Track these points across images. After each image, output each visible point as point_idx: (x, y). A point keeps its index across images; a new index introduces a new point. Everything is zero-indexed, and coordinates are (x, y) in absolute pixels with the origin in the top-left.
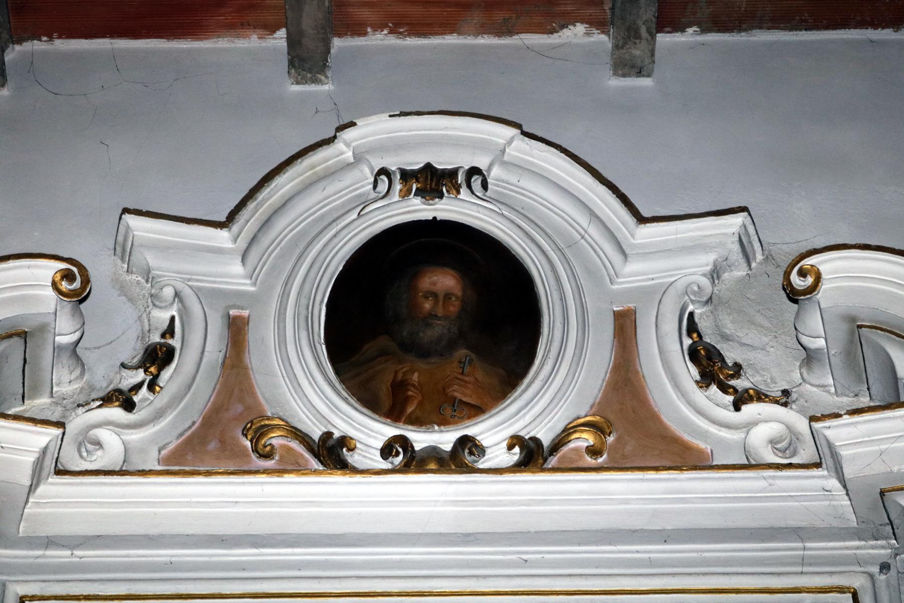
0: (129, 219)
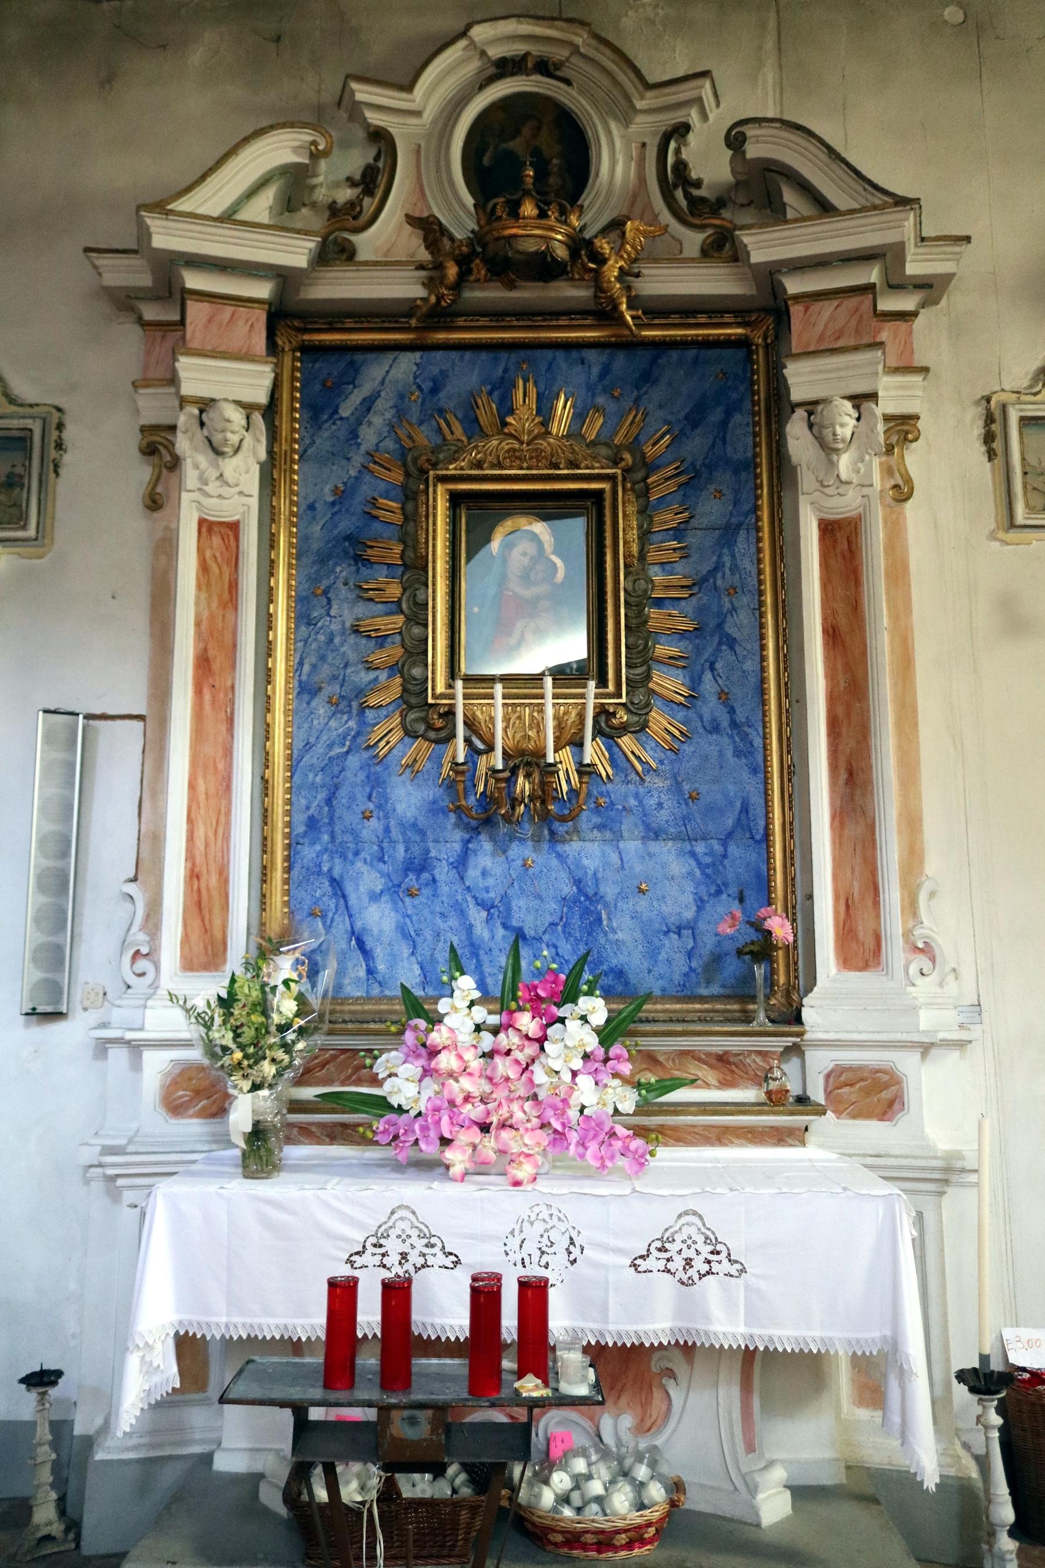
0: (354, 85)
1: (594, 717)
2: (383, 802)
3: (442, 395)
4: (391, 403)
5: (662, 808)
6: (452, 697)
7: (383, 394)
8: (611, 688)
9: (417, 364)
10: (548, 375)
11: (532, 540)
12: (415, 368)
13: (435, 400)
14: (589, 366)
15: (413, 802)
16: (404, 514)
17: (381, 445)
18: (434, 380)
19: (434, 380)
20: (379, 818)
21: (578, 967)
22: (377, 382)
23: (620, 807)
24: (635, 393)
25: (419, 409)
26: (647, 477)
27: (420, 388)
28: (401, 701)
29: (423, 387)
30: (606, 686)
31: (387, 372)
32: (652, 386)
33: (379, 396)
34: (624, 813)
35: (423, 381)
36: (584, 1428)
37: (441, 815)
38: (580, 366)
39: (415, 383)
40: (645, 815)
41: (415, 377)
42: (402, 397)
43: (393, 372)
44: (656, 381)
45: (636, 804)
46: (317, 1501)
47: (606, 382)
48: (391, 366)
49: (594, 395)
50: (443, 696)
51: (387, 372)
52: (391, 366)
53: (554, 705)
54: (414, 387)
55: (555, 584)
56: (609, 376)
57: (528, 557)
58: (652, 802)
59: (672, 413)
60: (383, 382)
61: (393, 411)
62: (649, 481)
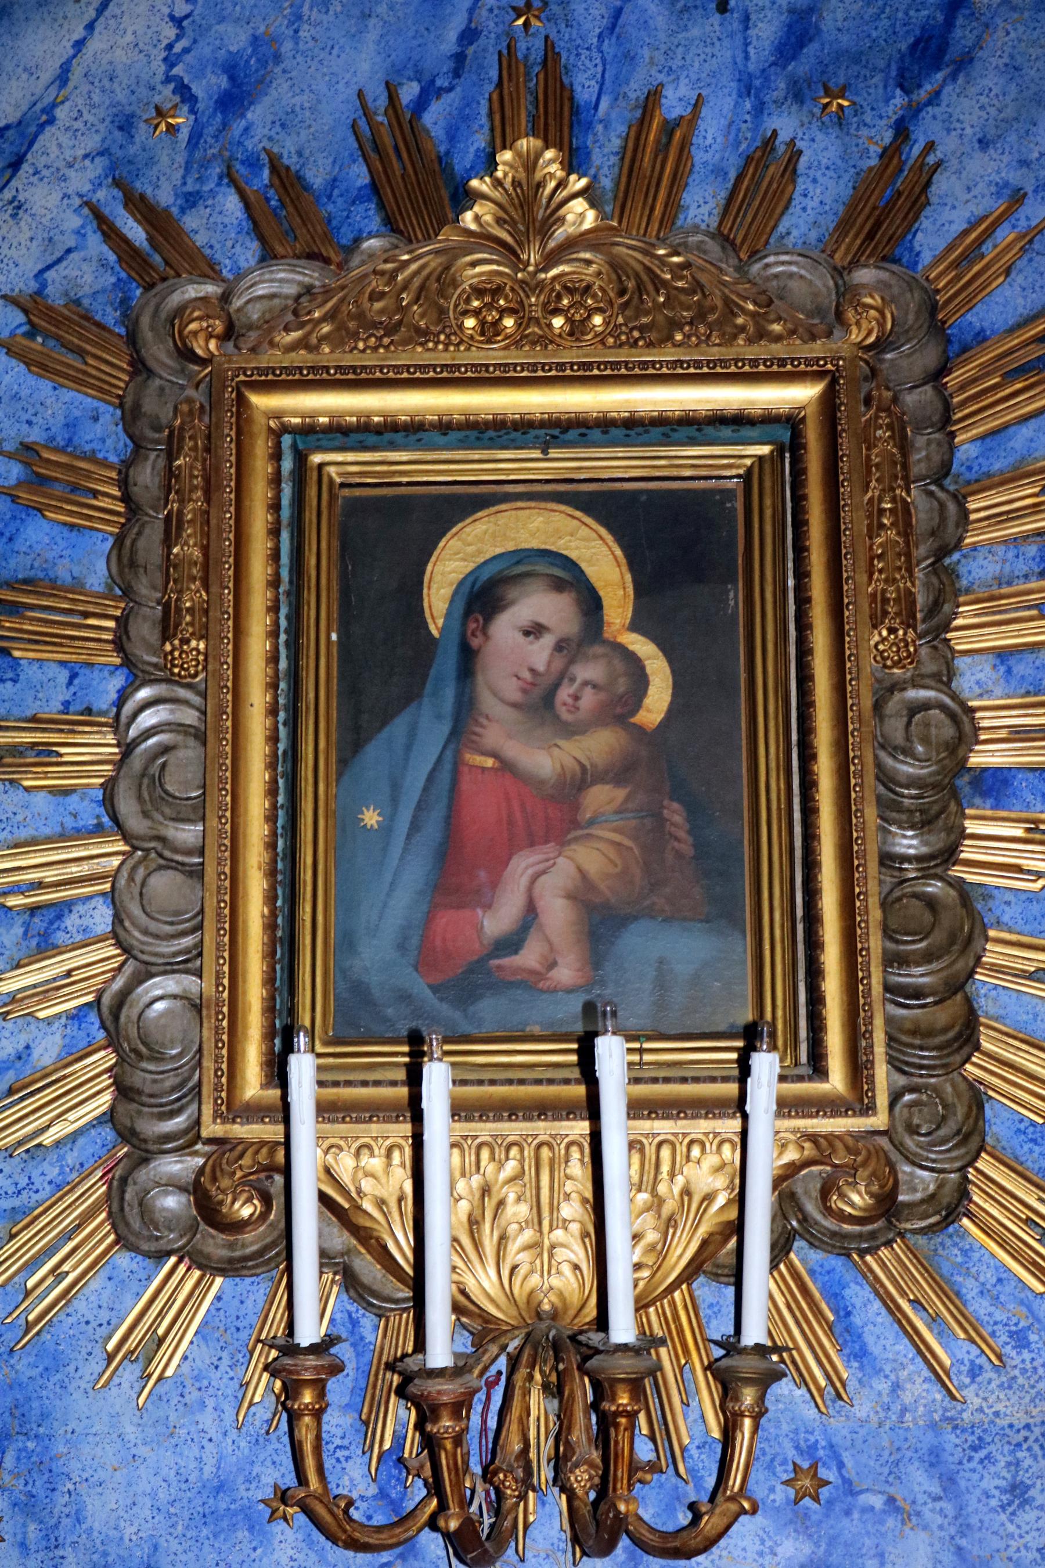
1: (777, 1182)
2: (39, 1488)
3: (257, 114)
4: (92, 142)
5: (1026, 1502)
6: (284, 1112)
7: (61, 113)
8: (837, 1081)
9: (178, 22)
10: (609, 47)
11: (558, 585)
12: (170, 32)
13: (237, 127)
14: (747, 18)
15: (144, 1486)
16: (126, 498)
17: (50, 275)
18: (231, 68)
19: (231, 68)
20: (23, 1545)
21: (447, 766)
22: (47, 74)
23: (877, 1502)
24: (899, 99)
25: (180, 159)
26: (943, 370)
27: (184, 92)
28: (108, 1133)
29: (197, 89)
30: (818, 1068)
31: (79, 45)
32: (953, 77)
33: (51, 121)
34: (891, 1522)
35: (200, 74)
36: (495, 694)
37: (242, 1534)
38: (716, 19)
39: (168, 79)
40: (965, 1530)
41: (170, 62)
42: (125, 124)
43: (96, 44)
44: (964, 63)
45: (936, 1489)
46: (652, 727)
47: (802, 66)
48: (90, 27)
49: (759, 109)
50: (255, 1112)
51: (79, 45)
52: (90, 27)
53: (634, 1145)
54: (168, 90)
55: (640, 729)
56: (811, 49)
57: (548, 641)
58: (989, 1483)
59: (1024, 163)
60: (63, 77)
61: (96, 168)
62: (952, 380)
